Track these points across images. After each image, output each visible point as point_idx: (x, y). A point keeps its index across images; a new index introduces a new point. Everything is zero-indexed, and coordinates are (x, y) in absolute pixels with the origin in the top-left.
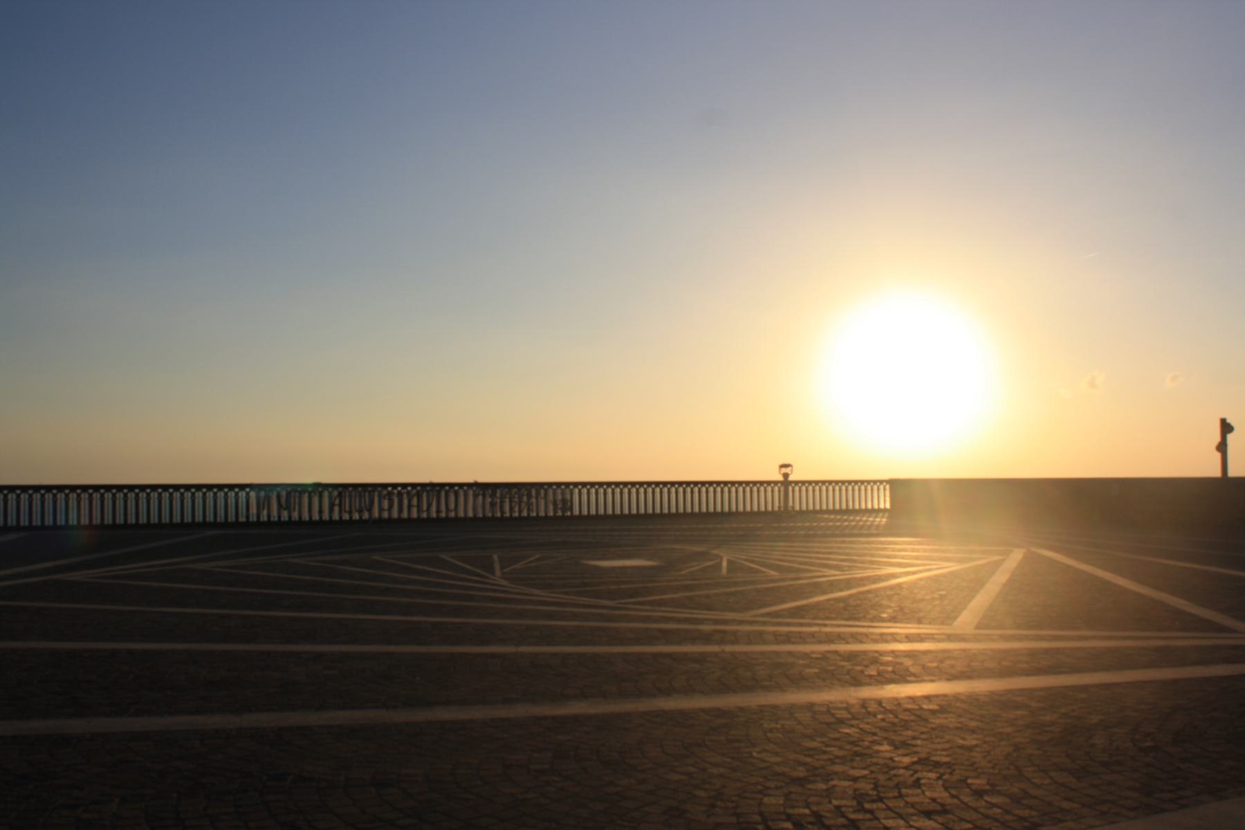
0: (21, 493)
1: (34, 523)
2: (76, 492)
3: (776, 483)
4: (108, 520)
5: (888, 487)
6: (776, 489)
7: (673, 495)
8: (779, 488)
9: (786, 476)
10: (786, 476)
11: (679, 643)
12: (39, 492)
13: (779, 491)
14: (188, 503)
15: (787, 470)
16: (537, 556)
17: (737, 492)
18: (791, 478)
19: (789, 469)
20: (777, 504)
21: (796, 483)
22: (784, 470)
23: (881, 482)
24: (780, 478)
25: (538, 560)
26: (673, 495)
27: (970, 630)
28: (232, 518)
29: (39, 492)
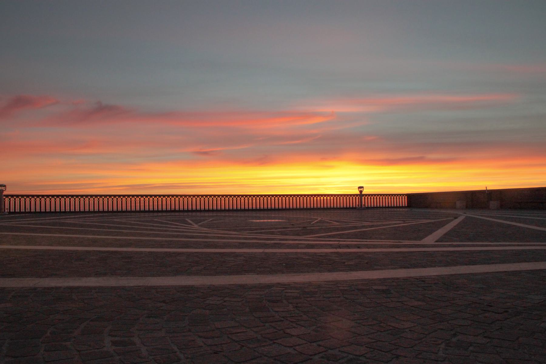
0: (6, 198)
1: (22, 211)
2: (97, 198)
3: (357, 195)
4: (82, 209)
5: (406, 197)
6: (357, 198)
7: (369, 199)
8: (359, 197)
9: (361, 192)
10: (361, 192)
11: (122, 230)
12: (93, 197)
13: (405, 198)
14: (110, 202)
15: (362, 189)
16: (211, 219)
17: (385, 198)
18: (363, 193)
19: (362, 189)
20: (357, 204)
21: (366, 195)
22: (360, 190)
23: (403, 195)
24: (358, 193)
25: (211, 221)
26: (369, 199)
27: (433, 243)
28: (164, 208)
29: (39, 197)
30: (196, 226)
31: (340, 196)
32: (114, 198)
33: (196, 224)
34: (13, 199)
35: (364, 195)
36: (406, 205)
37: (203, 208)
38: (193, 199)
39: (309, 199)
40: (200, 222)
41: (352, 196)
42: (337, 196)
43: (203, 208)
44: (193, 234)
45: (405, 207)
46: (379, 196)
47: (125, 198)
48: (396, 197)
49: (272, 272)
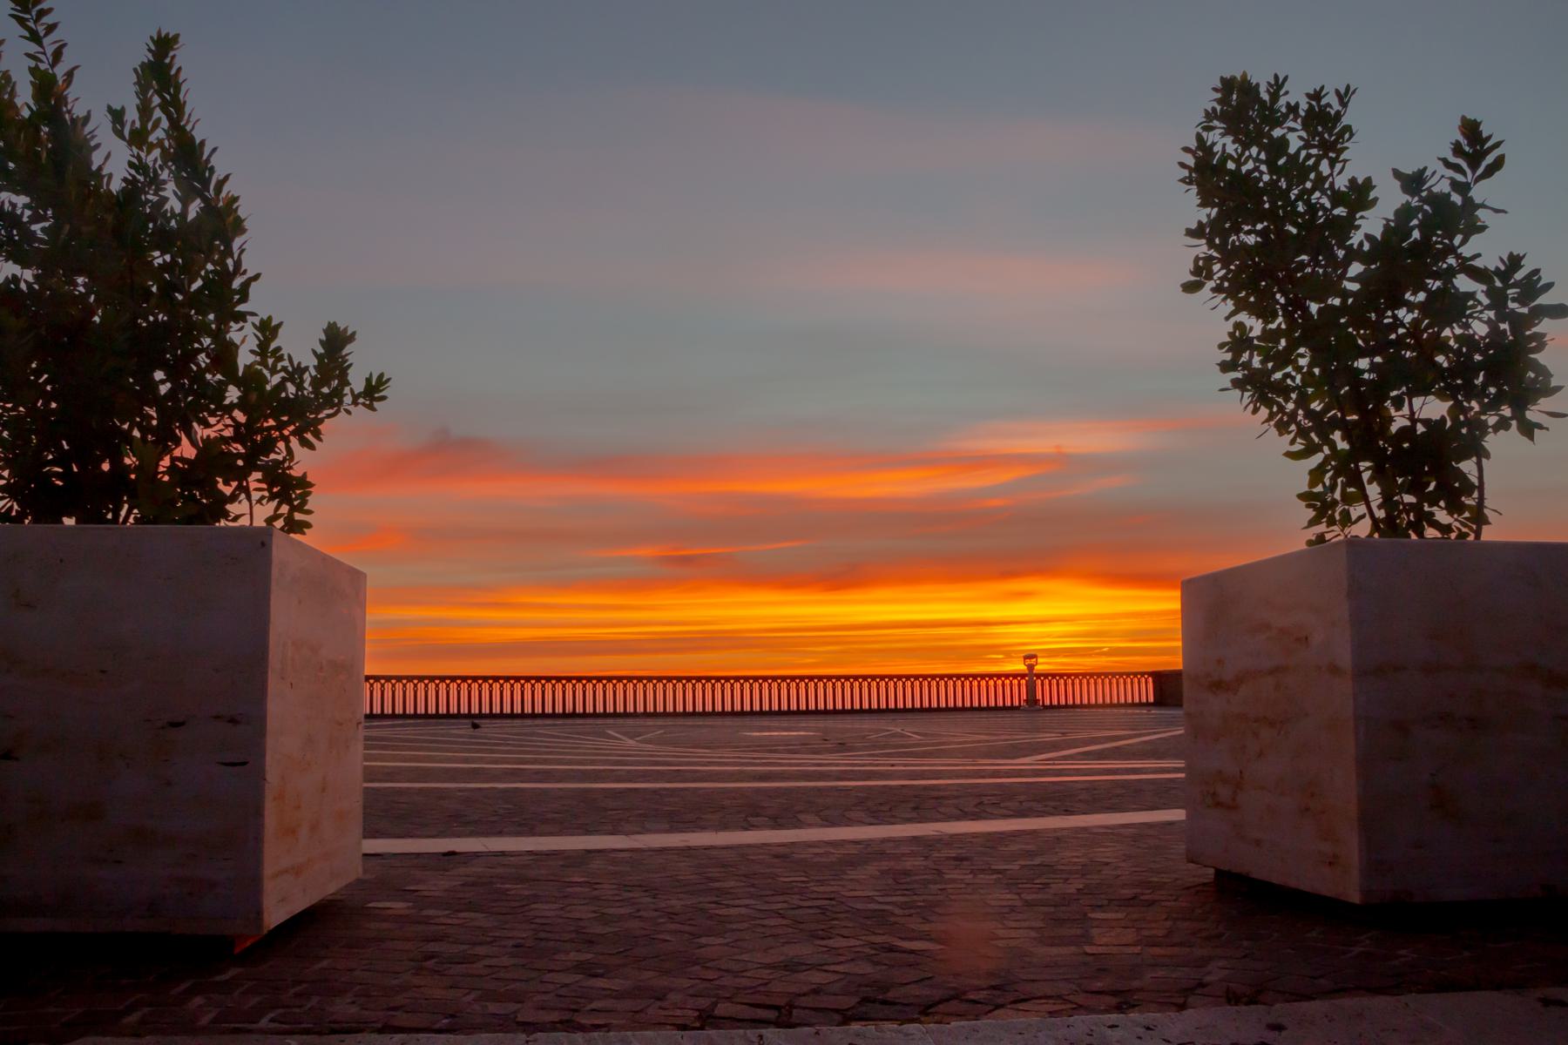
3: (1023, 676)
9: (1031, 667)
10: (1031, 667)
18: (1039, 668)
19: (1034, 660)
22: (1028, 662)
23: (1143, 674)
30: (631, 742)
31: (1139, 676)
32: (408, 684)
33: (631, 738)
34: (401, 684)
35: (1038, 676)
36: (1151, 700)
37: (640, 709)
38: (546, 687)
39: (739, 687)
40: (638, 736)
41: (979, 679)
42: (929, 679)
43: (640, 709)
44: (745, 768)
45: (1148, 704)
46: (995, 679)
47: (581, 684)
48: (1042, 681)
49: (742, 781)
